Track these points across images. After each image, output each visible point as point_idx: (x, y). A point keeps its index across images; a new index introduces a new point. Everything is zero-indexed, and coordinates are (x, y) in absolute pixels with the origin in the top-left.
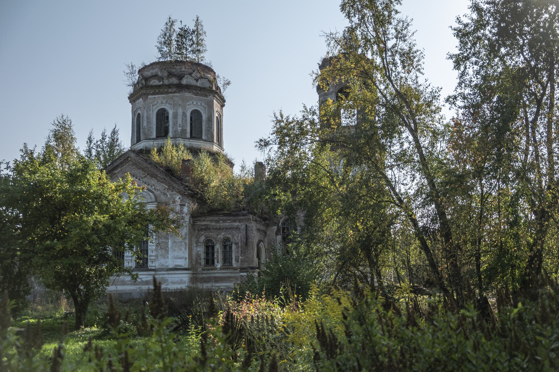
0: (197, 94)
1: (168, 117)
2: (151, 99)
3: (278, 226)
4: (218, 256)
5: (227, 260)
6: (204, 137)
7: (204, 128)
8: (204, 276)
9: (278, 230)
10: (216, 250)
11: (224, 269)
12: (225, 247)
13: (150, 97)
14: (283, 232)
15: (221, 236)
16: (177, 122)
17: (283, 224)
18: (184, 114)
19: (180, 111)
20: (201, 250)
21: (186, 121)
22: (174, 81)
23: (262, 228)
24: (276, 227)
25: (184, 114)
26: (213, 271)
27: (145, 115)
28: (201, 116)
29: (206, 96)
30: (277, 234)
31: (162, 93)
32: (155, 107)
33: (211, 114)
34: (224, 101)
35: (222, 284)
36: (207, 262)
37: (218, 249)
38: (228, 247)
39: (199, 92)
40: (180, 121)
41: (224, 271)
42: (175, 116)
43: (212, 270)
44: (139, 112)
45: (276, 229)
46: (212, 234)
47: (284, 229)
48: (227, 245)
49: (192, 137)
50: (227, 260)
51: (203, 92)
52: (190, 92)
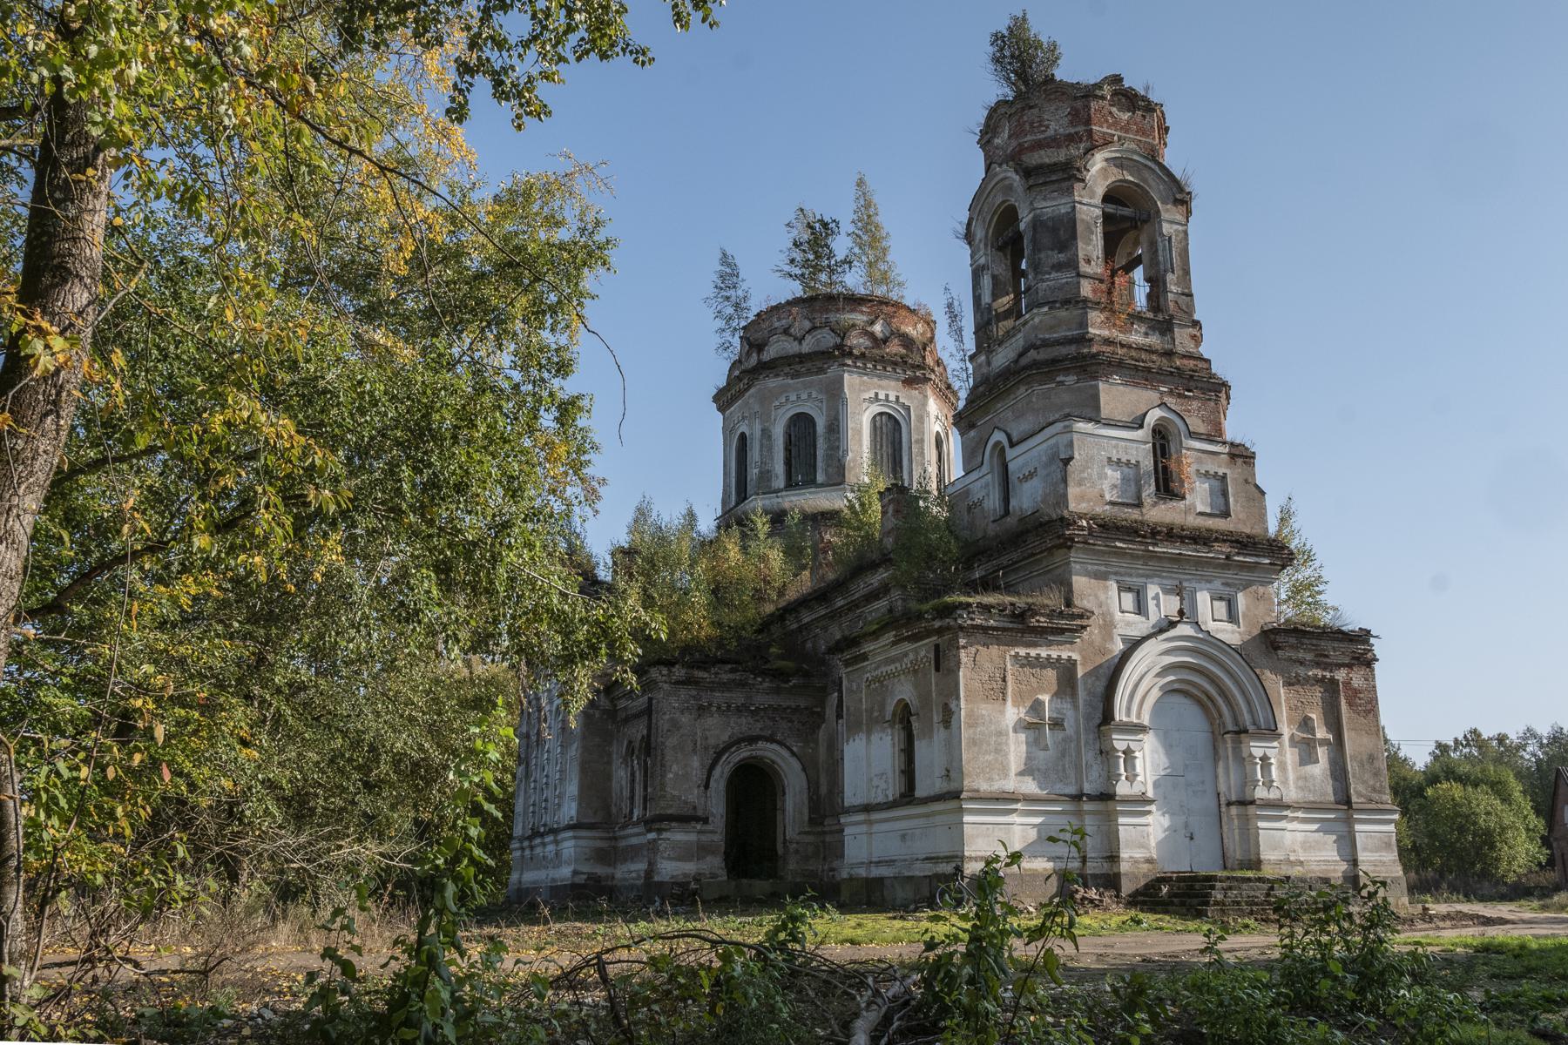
6: (820, 478)
7: (820, 453)
18: (766, 434)
27: (758, 433)
29: (821, 371)
32: (780, 411)
33: (836, 419)
39: (798, 367)
44: (743, 428)
49: (791, 484)
51: (809, 365)
52: (777, 375)
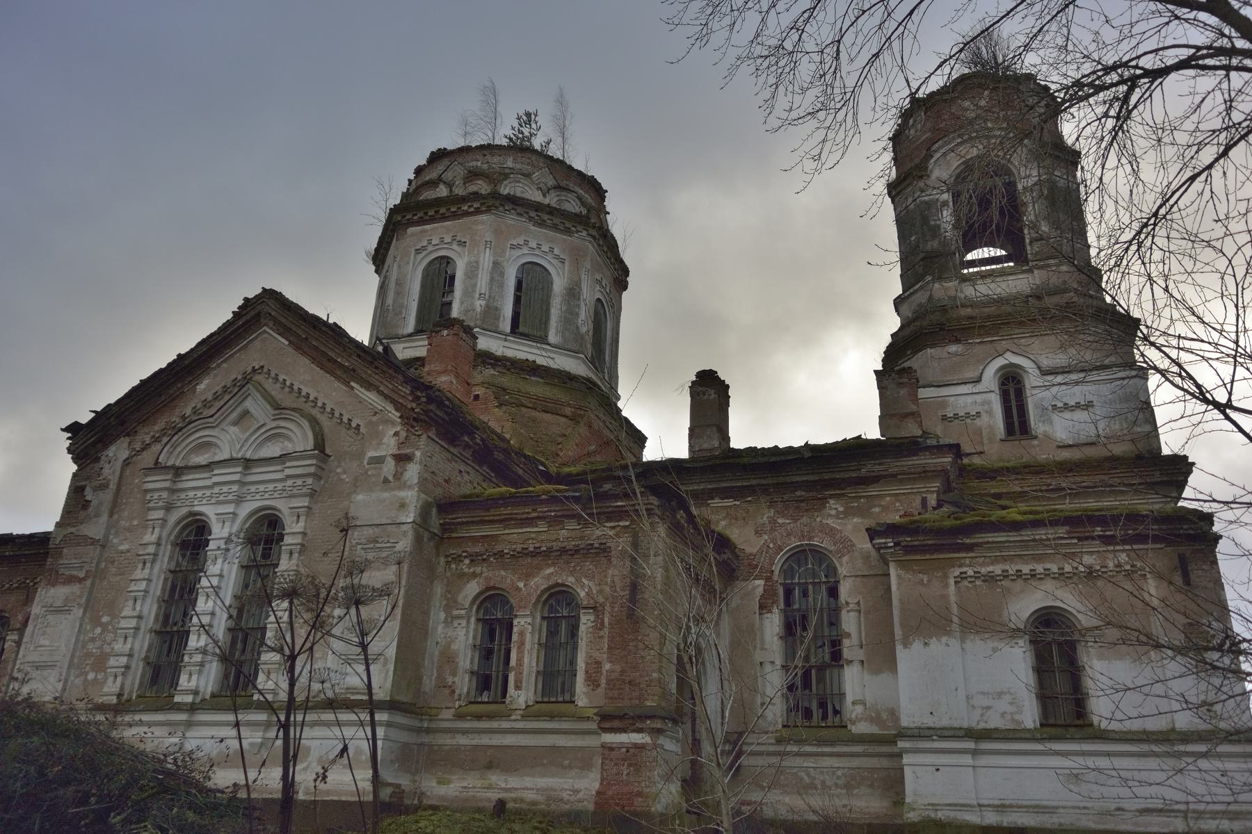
0: (541, 224)
1: (452, 278)
2: (413, 235)
3: (768, 579)
5: (555, 681)
6: (553, 337)
8: (463, 740)
10: (515, 637)
11: (538, 716)
12: (552, 622)
13: (411, 230)
14: (788, 602)
15: (539, 582)
16: (475, 286)
17: (787, 572)
19: (486, 259)
20: (461, 638)
21: (502, 286)
24: (761, 582)
25: (497, 267)
26: (495, 724)
30: (764, 607)
31: (444, 218)
34: (626, 272)
35: (528, 782)
36: (483, 682)
37: (522, 634)
39: (546, 217)
42: (472, 272)
43: (491, 717)
45: (760, 590)
46: (504, 578)
47: (788, 592)
48: (559, 604)
51: (557, 221)
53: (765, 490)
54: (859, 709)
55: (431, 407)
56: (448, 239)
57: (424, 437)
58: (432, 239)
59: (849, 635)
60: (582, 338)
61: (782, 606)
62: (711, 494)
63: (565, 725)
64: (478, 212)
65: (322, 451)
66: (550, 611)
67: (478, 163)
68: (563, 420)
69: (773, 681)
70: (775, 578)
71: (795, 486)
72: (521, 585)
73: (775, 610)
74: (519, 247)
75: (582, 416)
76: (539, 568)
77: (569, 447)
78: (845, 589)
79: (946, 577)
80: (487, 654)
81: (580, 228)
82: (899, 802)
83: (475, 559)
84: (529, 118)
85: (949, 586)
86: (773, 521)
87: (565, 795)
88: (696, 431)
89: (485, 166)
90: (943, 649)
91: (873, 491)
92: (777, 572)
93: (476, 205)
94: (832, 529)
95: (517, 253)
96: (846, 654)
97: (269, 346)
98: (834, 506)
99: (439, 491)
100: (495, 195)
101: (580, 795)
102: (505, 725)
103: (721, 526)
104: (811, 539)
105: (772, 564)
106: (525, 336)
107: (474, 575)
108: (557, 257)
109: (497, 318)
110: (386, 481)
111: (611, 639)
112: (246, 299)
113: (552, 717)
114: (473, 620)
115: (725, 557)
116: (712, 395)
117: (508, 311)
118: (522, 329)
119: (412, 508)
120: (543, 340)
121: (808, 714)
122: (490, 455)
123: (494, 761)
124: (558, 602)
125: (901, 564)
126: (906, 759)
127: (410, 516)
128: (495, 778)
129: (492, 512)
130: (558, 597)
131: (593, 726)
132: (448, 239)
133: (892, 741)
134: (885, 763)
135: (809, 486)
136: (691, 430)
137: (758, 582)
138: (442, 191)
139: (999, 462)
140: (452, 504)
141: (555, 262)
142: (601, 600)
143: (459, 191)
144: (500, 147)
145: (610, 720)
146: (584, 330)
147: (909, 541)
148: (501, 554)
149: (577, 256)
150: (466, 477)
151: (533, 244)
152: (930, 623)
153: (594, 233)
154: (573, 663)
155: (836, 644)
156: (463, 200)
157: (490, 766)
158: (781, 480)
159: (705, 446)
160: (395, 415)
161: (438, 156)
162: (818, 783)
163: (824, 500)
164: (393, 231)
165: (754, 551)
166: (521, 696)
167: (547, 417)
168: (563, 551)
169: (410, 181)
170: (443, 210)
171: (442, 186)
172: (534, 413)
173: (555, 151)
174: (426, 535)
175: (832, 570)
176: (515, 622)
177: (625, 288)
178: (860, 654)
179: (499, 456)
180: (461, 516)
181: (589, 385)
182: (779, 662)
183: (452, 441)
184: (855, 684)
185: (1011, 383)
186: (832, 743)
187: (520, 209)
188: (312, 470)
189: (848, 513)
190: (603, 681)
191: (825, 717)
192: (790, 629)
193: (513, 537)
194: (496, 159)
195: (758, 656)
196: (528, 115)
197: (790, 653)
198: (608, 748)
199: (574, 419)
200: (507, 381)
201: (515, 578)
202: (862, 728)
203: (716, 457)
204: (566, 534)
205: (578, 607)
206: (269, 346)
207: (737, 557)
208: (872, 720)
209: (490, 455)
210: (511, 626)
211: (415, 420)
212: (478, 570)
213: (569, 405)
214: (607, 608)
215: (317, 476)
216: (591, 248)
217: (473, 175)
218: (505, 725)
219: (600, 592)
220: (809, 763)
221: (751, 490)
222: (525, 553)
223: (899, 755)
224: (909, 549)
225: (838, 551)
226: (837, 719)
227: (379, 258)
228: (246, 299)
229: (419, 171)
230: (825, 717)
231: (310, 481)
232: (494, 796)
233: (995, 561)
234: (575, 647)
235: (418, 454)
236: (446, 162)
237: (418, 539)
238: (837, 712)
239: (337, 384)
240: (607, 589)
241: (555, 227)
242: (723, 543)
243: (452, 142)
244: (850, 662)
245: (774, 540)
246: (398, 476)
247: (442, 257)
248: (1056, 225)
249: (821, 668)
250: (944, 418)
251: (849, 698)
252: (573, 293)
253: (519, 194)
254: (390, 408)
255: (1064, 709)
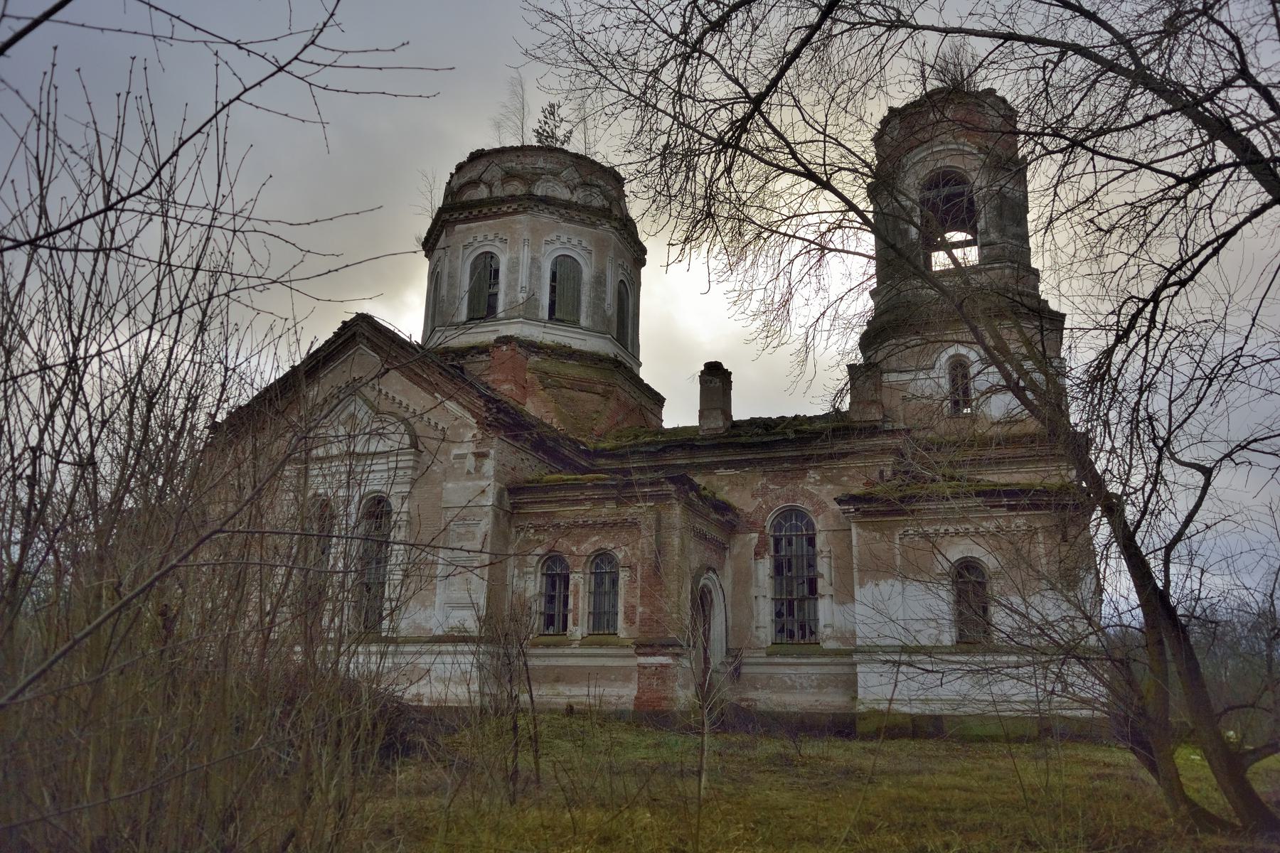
1: (497, 271)
2: (459, 232)
3: (762, 533)
4: (576, 605)
5: (602, 620)
6: (584, 321)
9: (762, 544)
10: (571, 588)
11: (591, 645)
12: (599, 577)
13: (459, 227)
14: (777, 550)
15: (588, 547)
17: (777, 526)
19: (525, 255)
20: (532, 586)
21: (539, 278)
22: (517, 188)
23: (713, 533)
24: (755, 536)
26: (560, 651)
28: (580, 272)
31: (486, 217)
36: (550, 621)
37: (576, 585)
38: (607, 579)
39: (573, 213)
40: (523, 278)
41: (590, 651)
42: (514, 266)
43: (556, 645)
46: (564, 545)
48: (603, 565)
50: (602, 620)
51: (584, 216)
53: (759, 462)
54: (829, 631)
55: (501, 416)
56: (491, 237)
57: (496, 439)
58: (477, 236)
59: (822, 576)
60: (609, 320)
61: (772, 553)
62: (717, 465)
63: (610, 651)
64: (516, 212)
65: (416, 448)
66: (597, 566)
67: (513, 164)
68: (596, 397)
69: (765, 612)
70: (767, 531)
71: (781, 460)
72: (574, 549)
73: (767, 556)
74: (552, 242)
75: (612, 392)
76: (587, 537)
77: (599, 419)
78: (820, 540)
79: (893, 534)
80: (551, 599)
81: (604, 221)
82: (855, 698)
83: (538, 529)
84: (552, 110)
85: (896, 541)
86: (765, 487)
87: (613, 700)
88: (706, 413)
89: (519, 167)
90: (889, 587)
91: (842, 464)
92: (768, 528)
93: (515, 206)
94: (811, 493)
95: (550, 248)
96: (820, 590)
97: (365, 360)
98: (813, 475)
99: (508, 478)
100: (530, 196)
101: (623, 700)
102: (568, 651)
103: (723, 495)
104: (794, 501)
105: (764, 521)
106: (558, 320)
107: (540, 542)
108: (585, 249)
109: (537, 308)
110: (469, 473)
111: (643, 590)
112: (344, 323)
113: (601, 645)
114: (539, 574)
115: (727, 518)
116: (717, 383)
117: (545, 300)
118: (557, 315)
119: (490, 494)
120: (575, 323)
121: (791, 635)
122: (544, 444)
123: (561, 676)
124: (602, 561)
125: (860, 524)
126: (859, 668)
127: (489, 500)
128: (561, 688)
129: (550, 494)
130: (602, 557)
131: (632, 652)
132: (491, 237)
133: (849, 654)
134: (846, 669)
135: (793, 460)
136: (701, 412)
137: (754, 535)
138: (482, 192)
139: (972, 397)
140: (519, 489)
141: (583, 253)
142: (634, 560)
143: (498, 192)
144: (531, 148)
145: (644, 647)
146: (609, 313)
147: (866, 506)
148: (558, 526)
149: (601, 245)
150: (527, 463)
151: (564, 239)
152: (879, 569)
153: (616, 224)
154: (615, 606)
155: (812, 584)
156: (502, 201)
157: (558, 680)
158: (772, 455)
159: (713, 426)
160: (472, 421)
161: (477, 156)
162: (795, 688)
163: (805, 471)
164: (443, 227)
165: (750, 510)
166: (578, 631)
167: (583, 395)
168: (605, 524)
169: (452, 175)
170: (485, 210)
171: (482, 186)
172: (573, 393)
173: (575, 146)
174: (501, 513)
175: (810, 525)
176: (571, 577)
177: (644, 264)
178: (830, 590)
179: (550, 444)
180: (526, 498)
181: (617, 364)
182: (769, 595)
183: (515, 438)
184: (826, 611)
185: (959, 368)
186: (808, 656)
187: (552, 209)
188: (411, 464)
189: (825, 480)
190: (638, 619)
191: (803, 637)
192: (778, 569)
193: (567, 513)
194: (528, 160)
195: (753, 592)
196: (552, 106)
197: (778, 588)
198: (642, 667)
199: (605, 396)
200: (549, 365)
201: (569, 544)
202: (830, 645)
203: (720, 436)
204: (608, 510)
205: (617, 565)
206: (365, 360)
207: (738, 515)
208: (838, 639)
209: (544, 444)
210: (567, 577)
211: (489, 425)
212: (541, 537)
213: (600, 383)
214: (639, 568)
215: (414, 468)
216: (613, 237)
217: (509, 176)
218: (568, 651)
219: (634, 554)
220: (787, 670)
221: (749, 462)
222: (576, 525)
223: (854, 665)
224: (866, 514)
225: (815, 511)
226: (813, 638)
227: (430, 245)
228: (344, 323)
229: (460, 167)
230: (803, 637)
231: (409, 472)
232: (563, 701)
233: (930, 522)
234: (616, 594)
235: (492, 452)
236: (484, 162)
237: (496, 516)
238: (812, 633)
239: (423, 394)
240: (639, 553)
241: (582, 222)
242: (724, 508)
243: (490, 142)
244: (822, 596)
245: (766, 502)
246: (478, 469)
247: (487, 253)
248: (1002, 231)
249: (802, 600)
250: (904, 398)
251: (821, 623)
252: (599, 281)
253: (550, 193)
254: (468, 415)
255: (973, 628)
